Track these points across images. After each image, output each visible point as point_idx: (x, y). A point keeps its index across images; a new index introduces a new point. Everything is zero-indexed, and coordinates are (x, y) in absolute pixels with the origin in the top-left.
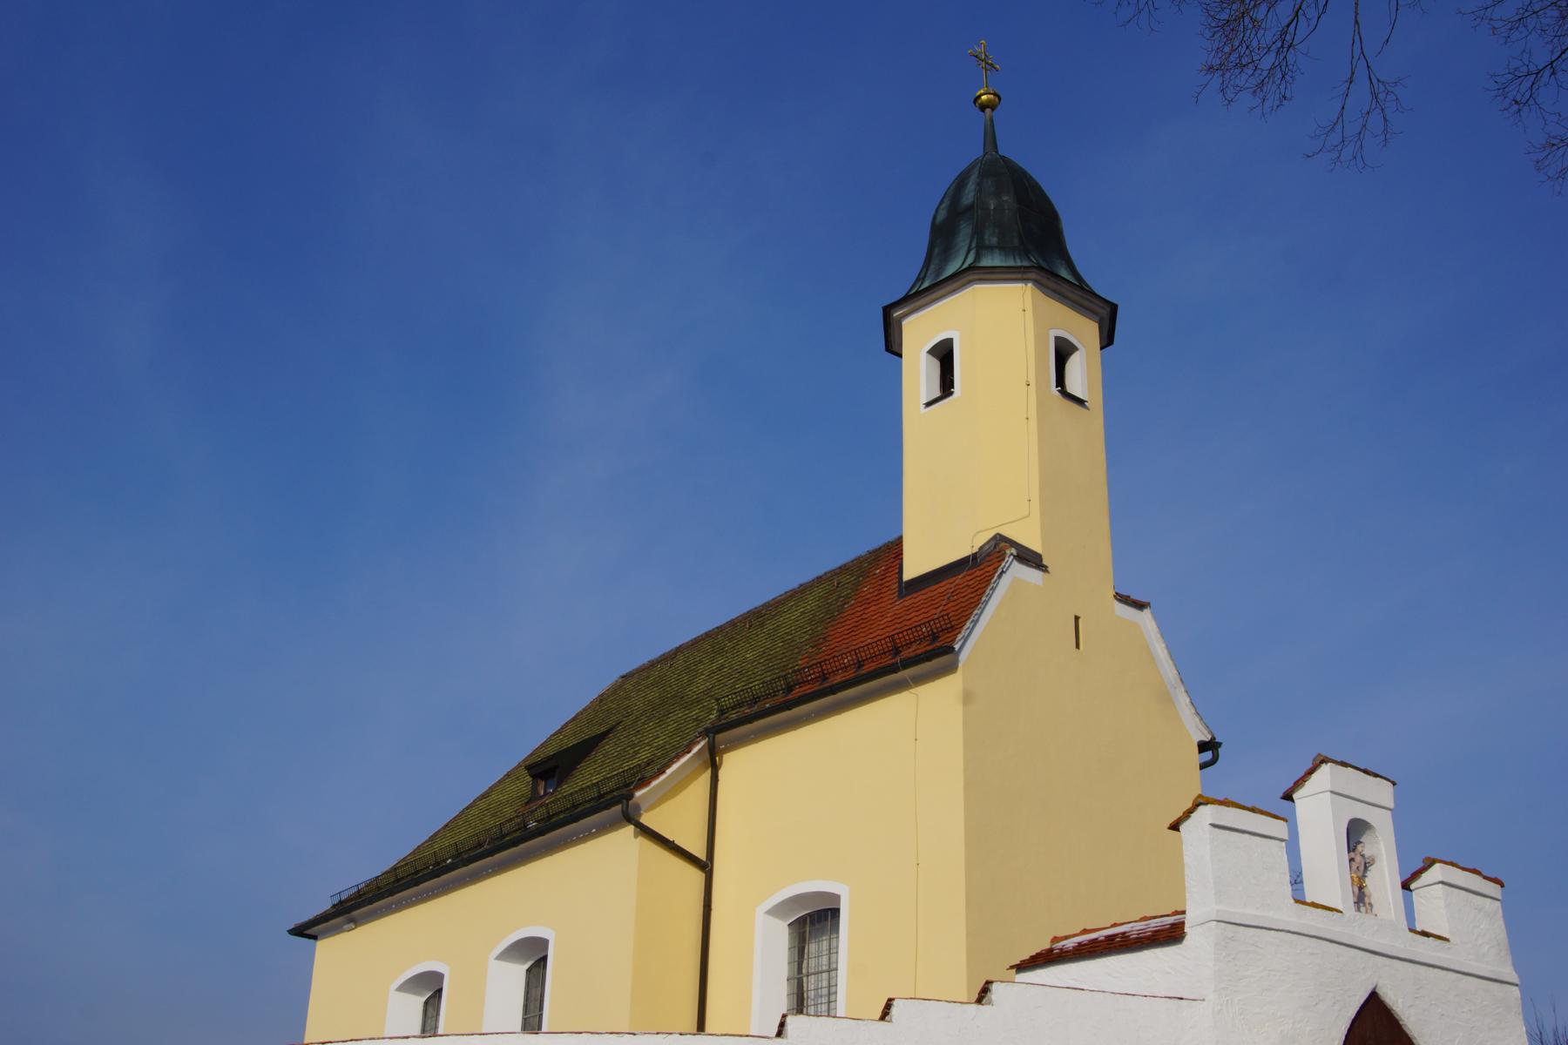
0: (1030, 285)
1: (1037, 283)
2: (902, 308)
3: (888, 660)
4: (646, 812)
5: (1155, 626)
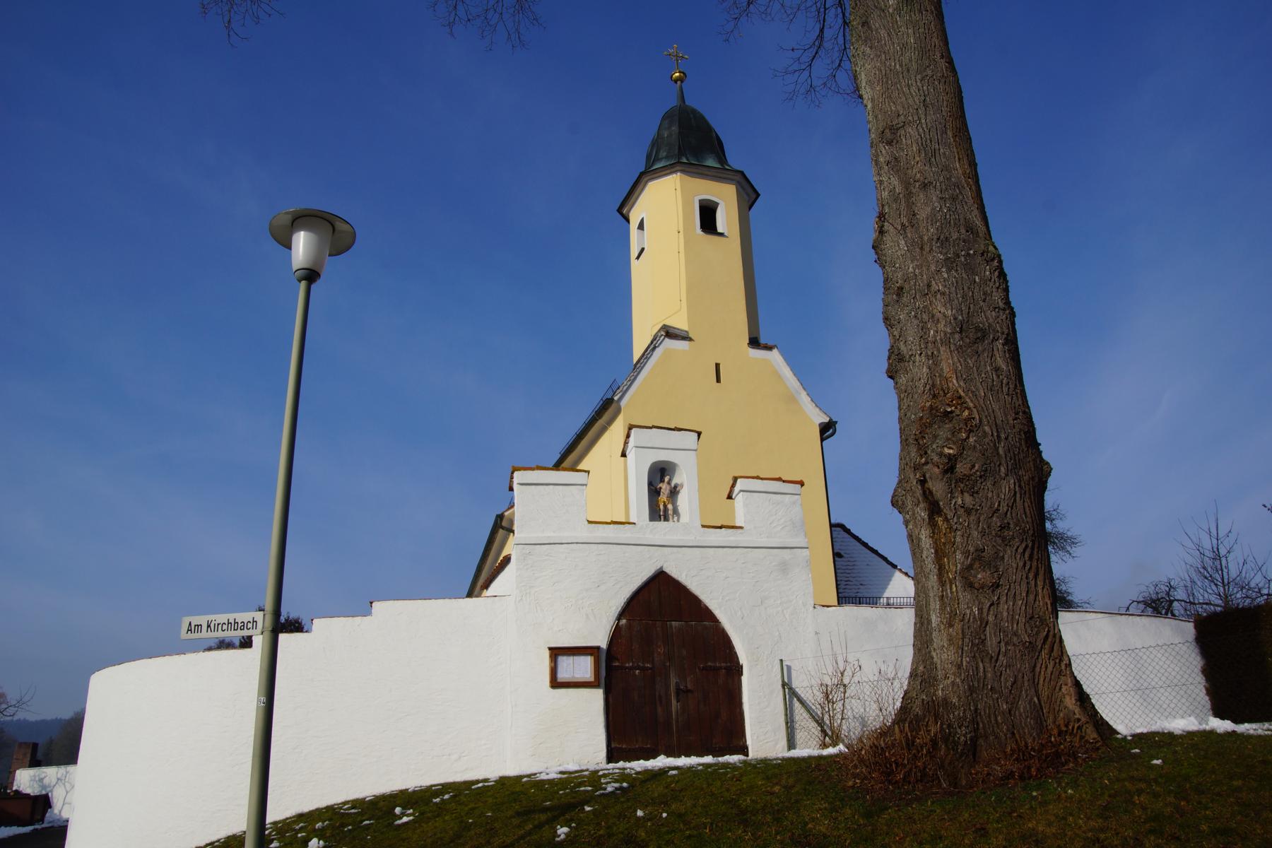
0: (679, 174)
1: (683, 171)
5: (781, 358)
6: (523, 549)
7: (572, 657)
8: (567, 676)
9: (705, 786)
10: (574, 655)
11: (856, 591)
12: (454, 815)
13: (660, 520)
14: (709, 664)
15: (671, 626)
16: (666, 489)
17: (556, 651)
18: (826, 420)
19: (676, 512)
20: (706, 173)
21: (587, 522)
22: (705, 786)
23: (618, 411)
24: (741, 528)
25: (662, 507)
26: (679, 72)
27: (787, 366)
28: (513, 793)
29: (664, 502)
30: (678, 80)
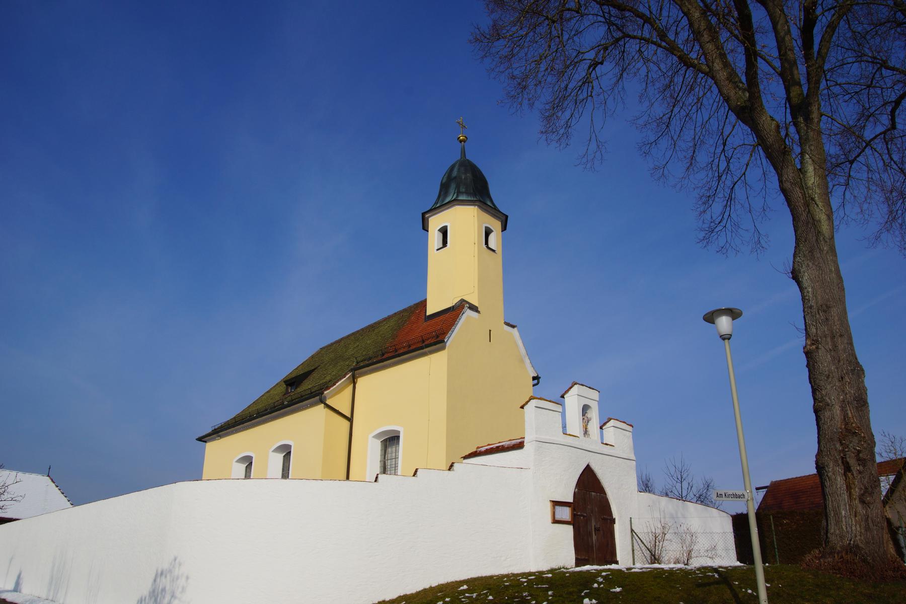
1: (479, 207)
3: (420, 345)
10: (562, 506)
18: (536, 375)
20: (489, 210)
30: (462, 141)
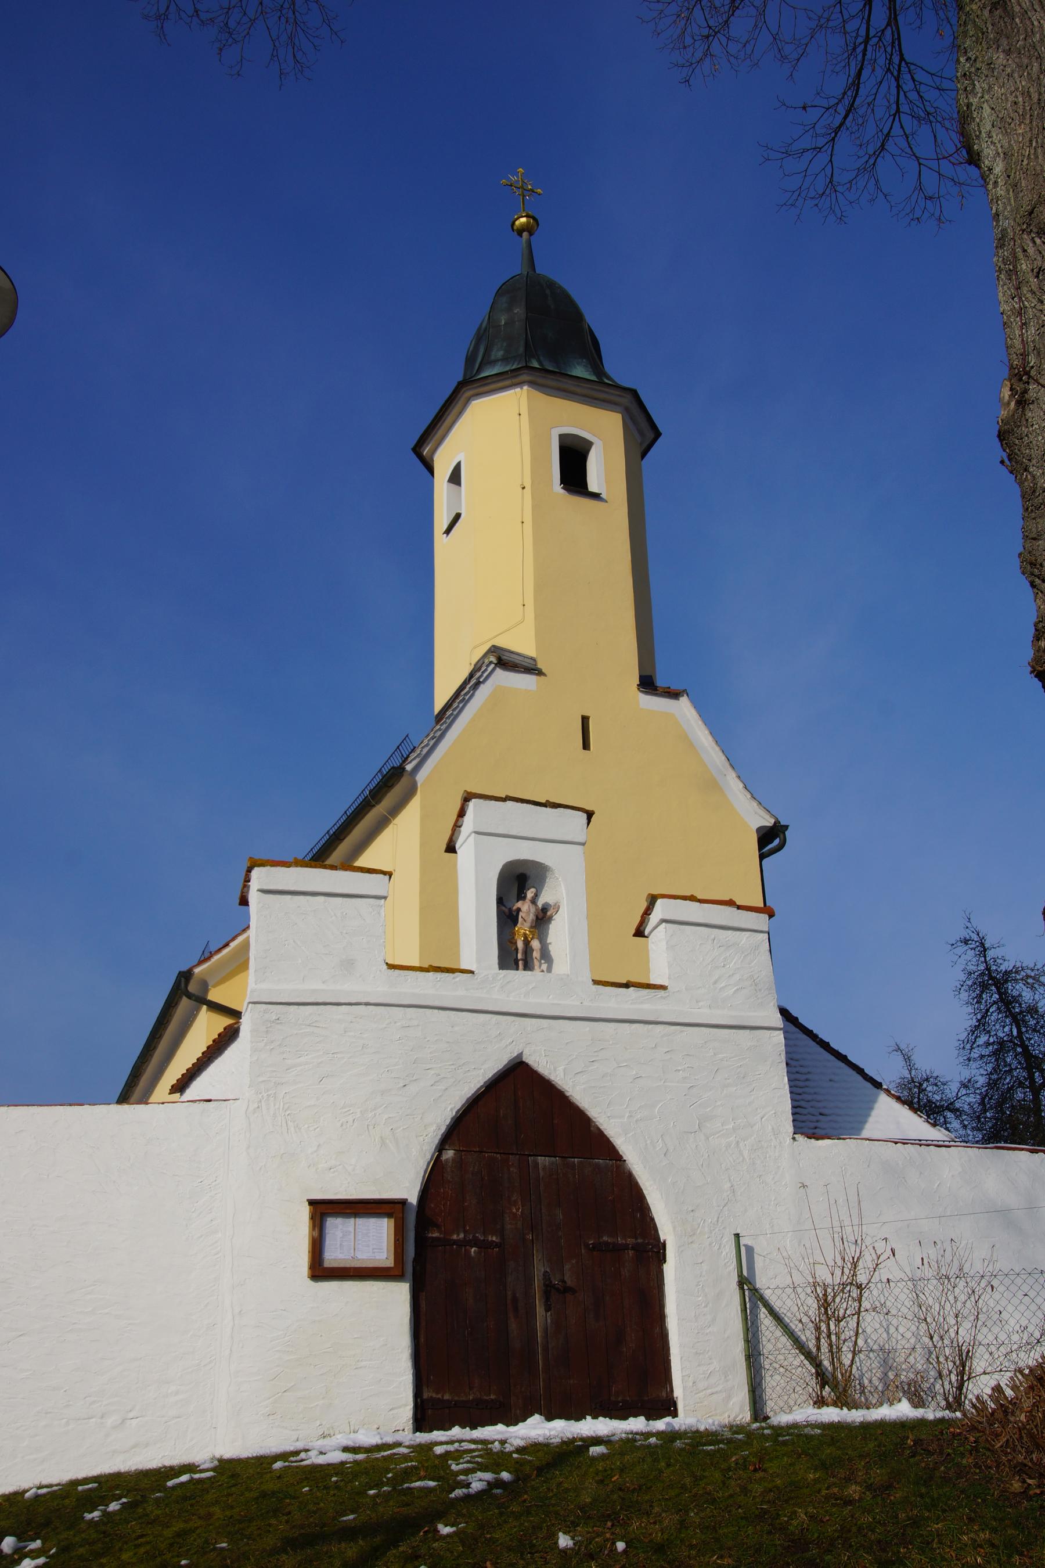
0: (525, 388)
1: (532, 384)
2: (428, 445)
4: (214, 986)
6: (265, 1012)
7: (352, 1220)
8: (341, 1256)
9: (688, 1480)
10: (356, 1215)
11: (813, 1125)
12: (142, 1550)
13: (517, 969)
14: (605, 1238)
15: (536, 1164)
16: (528, 912)
17: (323, 1206)
18: (769, 822)
19: (546, 956)
20: (573, 388)
21: (385, 967)
22: (688, 1480)
23: (411, 791)
24: (663, 988)
25: (520, 945)
26: (527, 216)
27: (703, 727)
28: (264, 1495)
29: (525, 936)
